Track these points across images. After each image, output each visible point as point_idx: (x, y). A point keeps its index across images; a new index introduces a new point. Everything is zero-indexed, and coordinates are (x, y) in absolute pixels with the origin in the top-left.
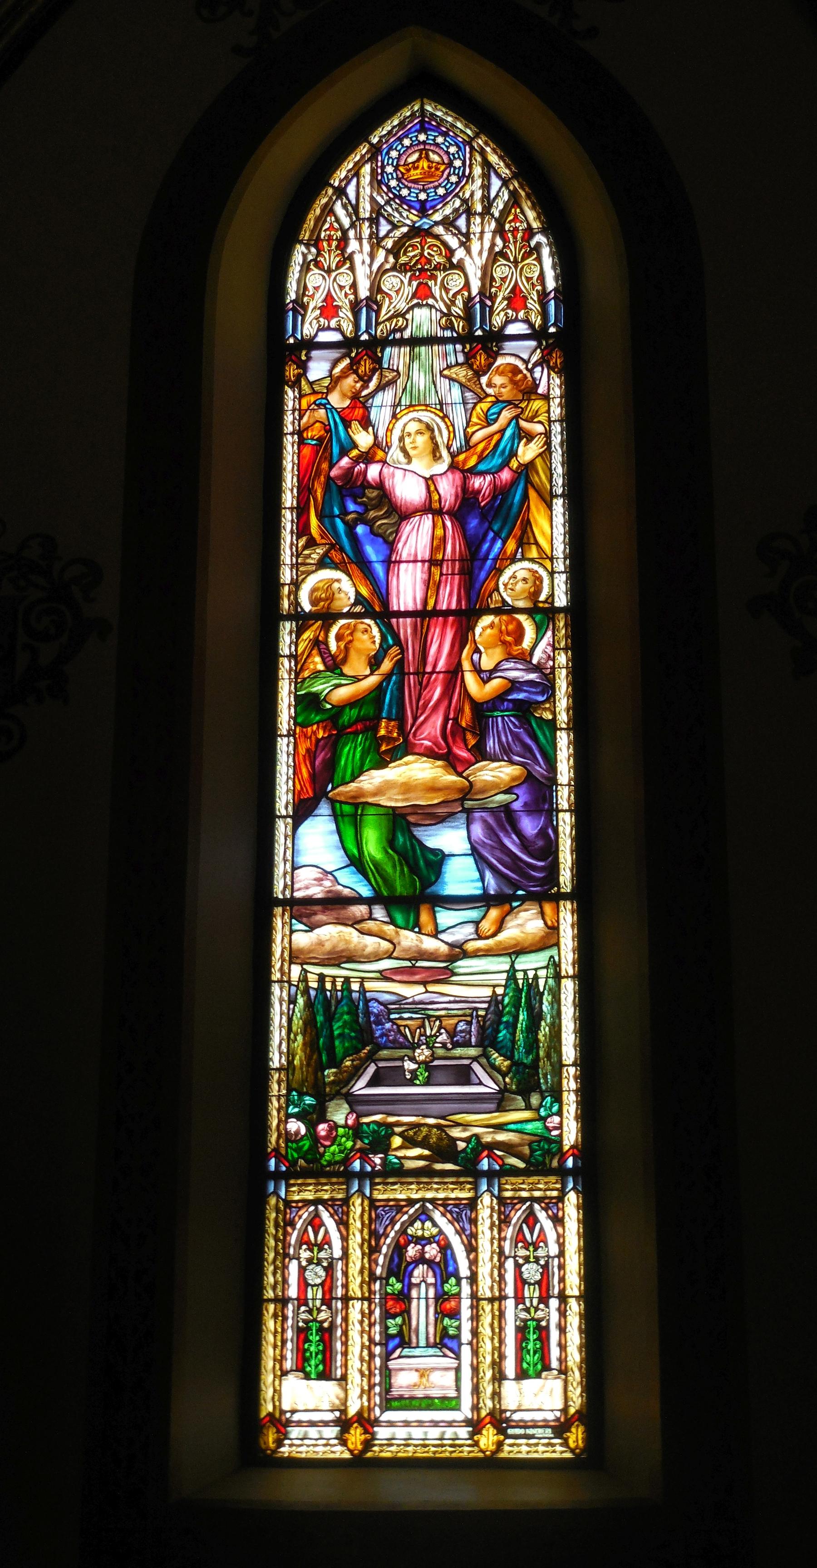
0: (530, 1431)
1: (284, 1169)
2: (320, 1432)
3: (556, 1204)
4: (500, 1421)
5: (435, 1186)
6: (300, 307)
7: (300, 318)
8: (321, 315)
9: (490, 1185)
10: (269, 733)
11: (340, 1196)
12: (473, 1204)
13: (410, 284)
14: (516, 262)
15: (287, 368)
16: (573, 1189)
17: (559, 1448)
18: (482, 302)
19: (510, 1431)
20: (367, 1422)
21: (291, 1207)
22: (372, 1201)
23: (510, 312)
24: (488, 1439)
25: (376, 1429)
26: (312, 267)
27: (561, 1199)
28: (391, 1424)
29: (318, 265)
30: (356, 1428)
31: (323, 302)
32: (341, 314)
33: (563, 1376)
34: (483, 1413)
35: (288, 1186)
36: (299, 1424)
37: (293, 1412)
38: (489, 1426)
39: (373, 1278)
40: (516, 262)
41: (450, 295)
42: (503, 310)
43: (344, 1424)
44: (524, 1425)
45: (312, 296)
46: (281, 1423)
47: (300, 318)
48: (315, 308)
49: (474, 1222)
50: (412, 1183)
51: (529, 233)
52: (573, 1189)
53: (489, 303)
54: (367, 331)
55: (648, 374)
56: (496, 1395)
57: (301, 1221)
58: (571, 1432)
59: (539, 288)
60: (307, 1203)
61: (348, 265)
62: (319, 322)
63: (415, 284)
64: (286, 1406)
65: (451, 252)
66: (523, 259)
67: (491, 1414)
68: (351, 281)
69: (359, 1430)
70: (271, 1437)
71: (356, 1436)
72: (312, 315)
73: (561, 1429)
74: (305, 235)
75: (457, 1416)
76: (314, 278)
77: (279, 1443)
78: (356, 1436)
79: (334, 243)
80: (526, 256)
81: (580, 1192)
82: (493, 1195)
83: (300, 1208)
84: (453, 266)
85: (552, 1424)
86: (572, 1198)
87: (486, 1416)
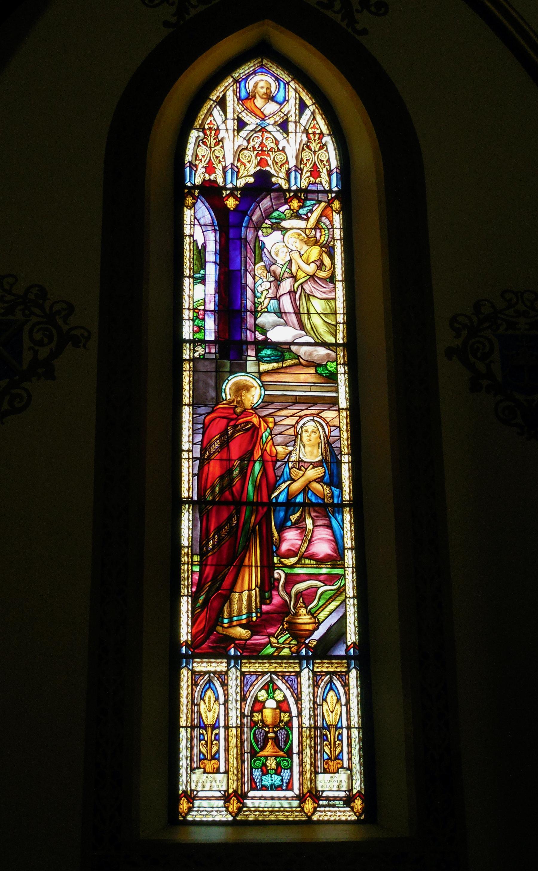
0: (332, 803)
1: (190, 653)
2: (281, 804)
3: (345, 676)
4: (315, 795)
5: (285, 665)
6: (193, 166)
7: (194, 172)
8: (311, 176)
9: (308, 664)
10: (178, 404)
11: (344, 670)
12: (298, 674)
13: (256, 159)
14: (315, 152)
15: (187, 199)
16: (354, 667)
17: (224, 813)
18: (232, 168)
19: (321, 803)
20: (242, 797)
21: (195, 675)
22: (193, 673)
23: (312, 179)
24: (309, 806)
25: (245, 801)
26: (201, 144)
27: (348, 672)
28: (253, 798)
29: (204, 143)
30: (234, 800)
31: (312, 168)
32: (217, 172)
33: (349, 772)
34: (355, 791)
35: (314, 664)
36: (201, 798)
37: (323, 791)
38: (308, 798)
39: (243, 715)
40: (315, 152)
41: (279, 165)
42: (308, 177)
43: (226, 798)
44: (328, 798)
45: (306, 164)
46: (191, 797)
47: (194, 172)
48: (307, 171)
49: (299, 683)
50: (265, 663)
51: (322, 134)
52: (354, 667)
53: (195, 169)
54: (231, 182)
55: (392, 219)
56: (314, 781)
57: (323, 683)
58: (230, 803)
59: (328, 167)
60: (327, 673)
61: (325, 149)
62: (310, 179)
63: (259, 158)
64: (320, 789)
65: (277, 142)
66: (215, 146)
67: (310, 791)
68: (327, 158)
69: (311, 802)
70: (184, 805)
71: (234, 805)
72: (201, 170)
73: (349, 801)
74: (197, 125)
75: (289, 794)
76: (203, 151)
77: (190, 809)
78: (309, 806)
79: (317, 136)
80: (321, 148)
81: (358, 670)
82: (309, 669)
83: (322, 676)
84: (279, 150)
85: (344, 799)
86: (353, 674)
87: (307, 793)
